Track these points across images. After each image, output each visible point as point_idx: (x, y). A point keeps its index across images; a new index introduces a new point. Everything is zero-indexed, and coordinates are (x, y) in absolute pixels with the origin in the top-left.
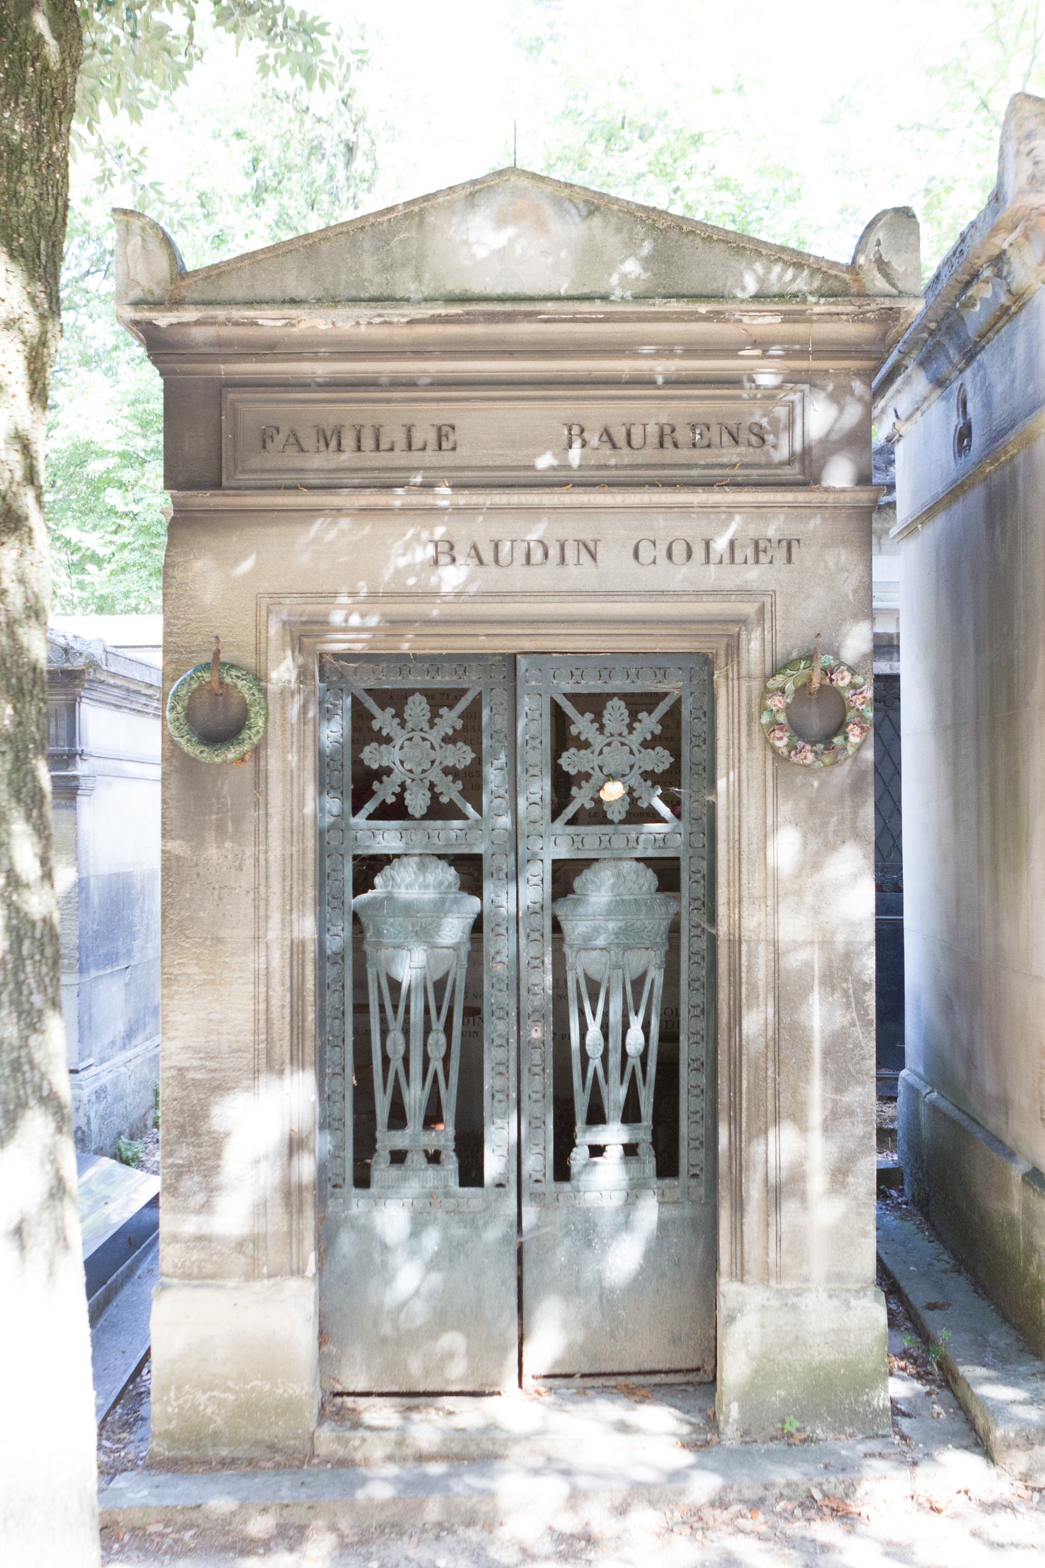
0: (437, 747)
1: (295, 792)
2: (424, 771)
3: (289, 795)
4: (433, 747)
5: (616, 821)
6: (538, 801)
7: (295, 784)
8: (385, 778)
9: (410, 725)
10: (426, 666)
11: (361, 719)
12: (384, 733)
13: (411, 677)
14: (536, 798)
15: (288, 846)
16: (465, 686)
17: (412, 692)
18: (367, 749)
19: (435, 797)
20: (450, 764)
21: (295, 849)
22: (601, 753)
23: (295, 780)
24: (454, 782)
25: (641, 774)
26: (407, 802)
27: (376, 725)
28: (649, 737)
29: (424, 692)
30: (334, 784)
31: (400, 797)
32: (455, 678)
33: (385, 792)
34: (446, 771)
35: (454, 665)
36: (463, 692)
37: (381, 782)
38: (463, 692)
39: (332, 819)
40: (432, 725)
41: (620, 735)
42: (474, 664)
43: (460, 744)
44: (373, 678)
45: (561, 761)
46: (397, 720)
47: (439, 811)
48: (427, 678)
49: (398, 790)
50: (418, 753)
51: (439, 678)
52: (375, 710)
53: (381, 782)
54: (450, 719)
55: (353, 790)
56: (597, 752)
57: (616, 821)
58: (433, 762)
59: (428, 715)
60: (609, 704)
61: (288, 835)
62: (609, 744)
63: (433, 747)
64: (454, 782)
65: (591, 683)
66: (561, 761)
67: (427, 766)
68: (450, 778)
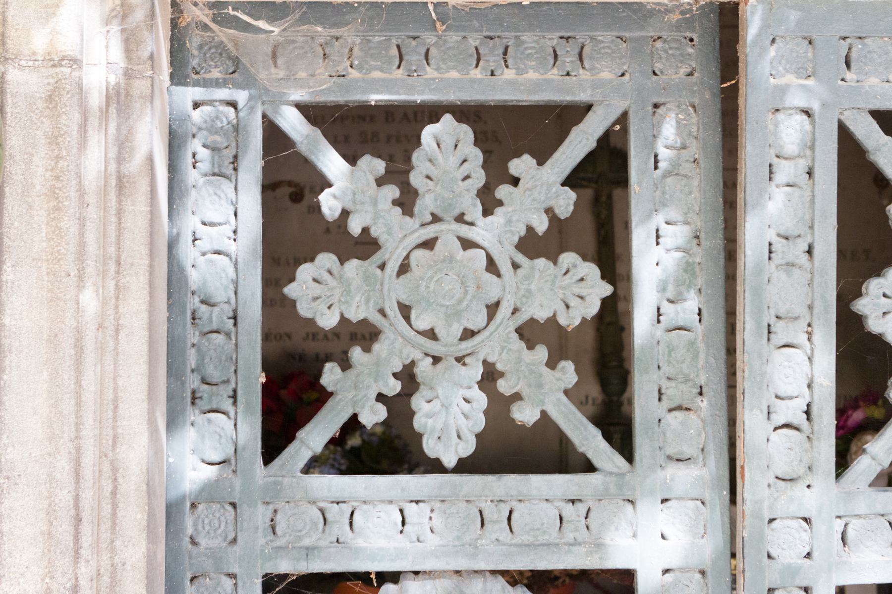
0: (505, 267)
1: (89, 396)
2: (468, 334)
3: (68, 406)
4: (492, 266)
5: (450, 461)
6: (800, 419)
7: (90, 377)
8: (356, 353)
9: (425, 204)
10: (474, 40)
11: (289, 188)
12: (355, 227)
13: (430, 72)
14: (792, 411)
15: (64, 562)
16: (583, 97)
17: (432, 113)
18: (305, 272)
19: (500, 406)
20: (542, 315)
21: (85, 571)
22: (404, 268)
23: (90, 357)
24: (551, 364)
25: (520, 331)
26: (419, 423)
27: (329, 203)
28: (541, 225)
29: (464, 113)
30: (214, 373)
31: (399, 406)
32: (554, 74)
33: (356, 393)
34: (530, 333)
35: (552, 39)
36: (577, 112)
37: (346, 365)
38: (577, 112)
39: (211, 472)
40: (489, 203)
41: (460, 219)
42: (606, 36)
43: (568, 258)
44: (322, 71)
45: (861, 306)
46: (392, 191)
47: (513, 450)
48: (476, 74)
49: (394, 387)
50: (450, 283)
51: (509, 74)
52: (331, 162)
53: (346, 365)
54: (543, 188)
55: (265, 386)
56: (393, 266)
57: (450, 461)
58: (493, 309)
59: (479, 178)
60: (429, 133)
61: (64, 528)
62: (428, 244)
63: (492, 266)
64: (551, 364)
65: (532, 75)
66: (861, 306)
67: (477, 319)
68: (542, 353)
